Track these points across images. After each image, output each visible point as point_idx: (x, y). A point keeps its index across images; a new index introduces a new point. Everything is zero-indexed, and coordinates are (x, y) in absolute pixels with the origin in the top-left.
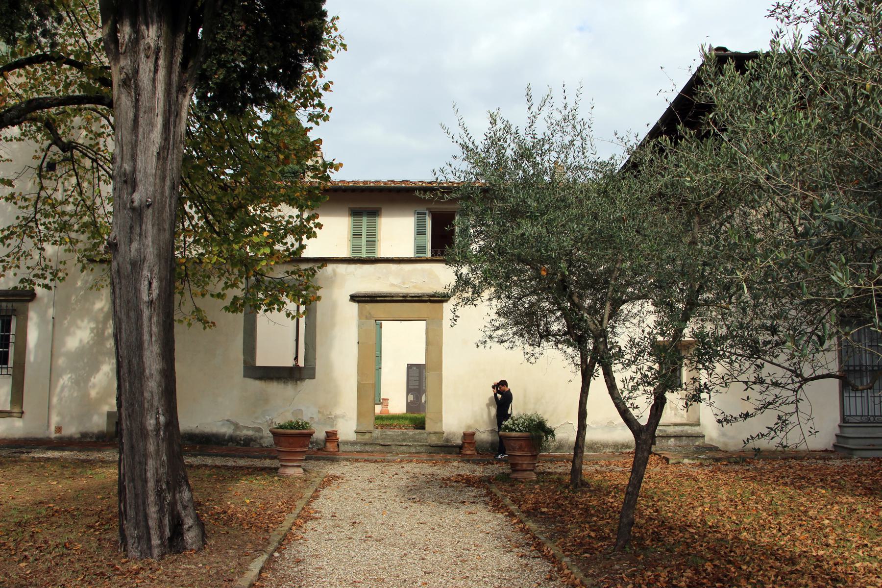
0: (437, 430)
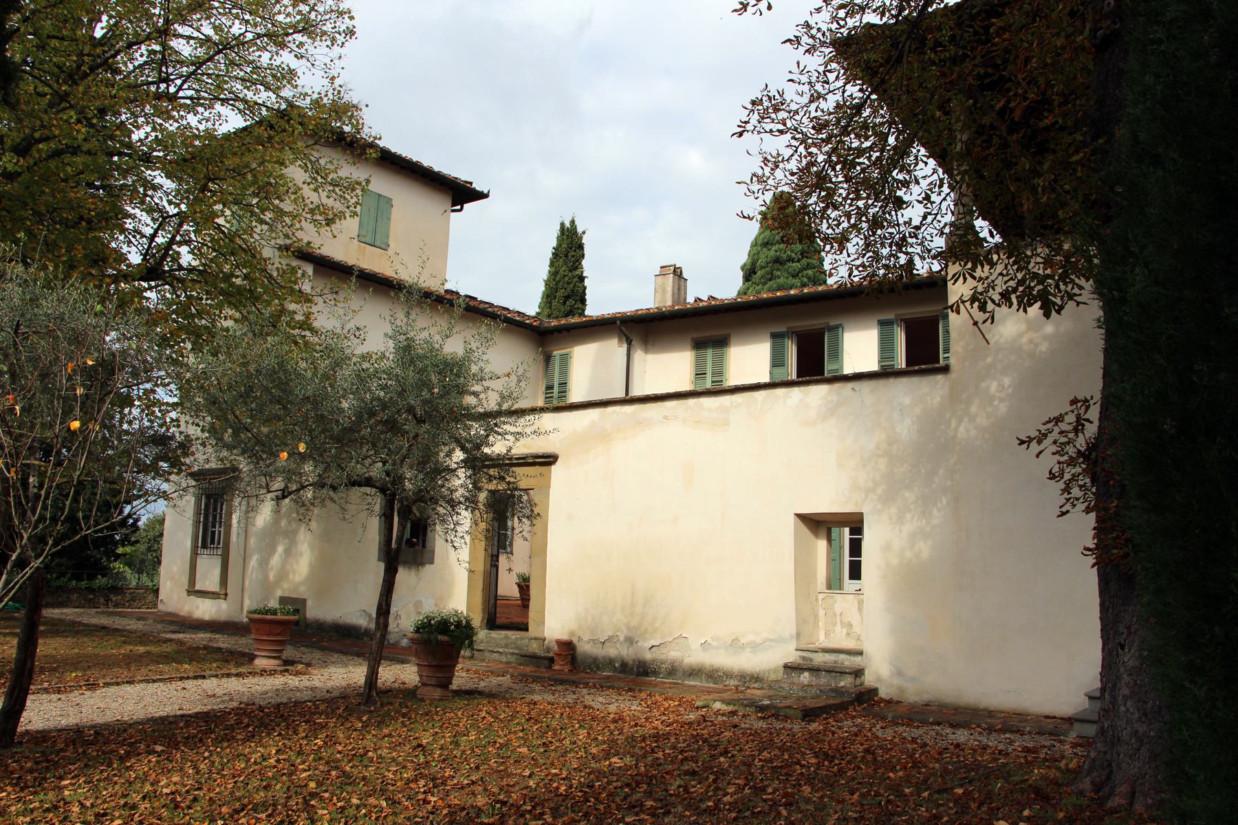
0: (539, 635)
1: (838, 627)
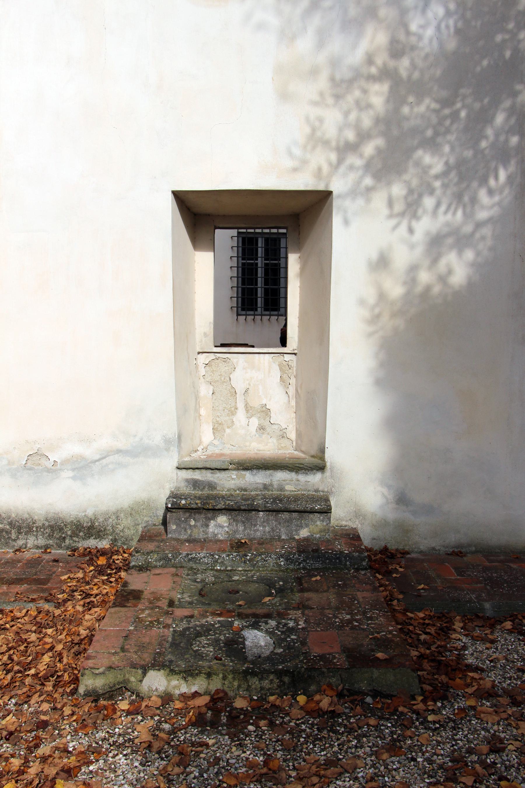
1: (241, 416)
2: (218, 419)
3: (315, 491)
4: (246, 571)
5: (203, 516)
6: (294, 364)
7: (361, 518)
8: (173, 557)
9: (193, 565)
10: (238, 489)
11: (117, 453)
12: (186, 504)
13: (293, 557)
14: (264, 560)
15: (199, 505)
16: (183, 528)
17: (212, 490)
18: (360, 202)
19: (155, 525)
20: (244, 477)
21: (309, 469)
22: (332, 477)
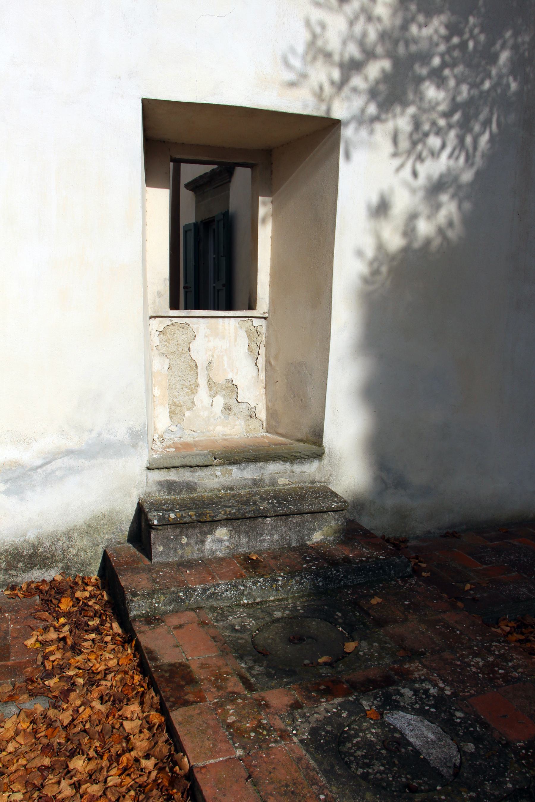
1: (203, 395)
2: (175, 400)
3: (311, 482)
4: (279, 600)
5: (197, 530)
6: (263, 330)
7: (359, 507)
8: (187, 596)
9: (214, 603)
10: (223, 489)
11: (67, 455)
12: (177, 517)
13: (332, 574)
14: (300, 584)
15: (194, 517)
16: (172, 549)
17: (191, 493)
18: (364, 133)
19: (119, 543)
20: (230, 473)
21: (306, 457)
22: (330, 464)
